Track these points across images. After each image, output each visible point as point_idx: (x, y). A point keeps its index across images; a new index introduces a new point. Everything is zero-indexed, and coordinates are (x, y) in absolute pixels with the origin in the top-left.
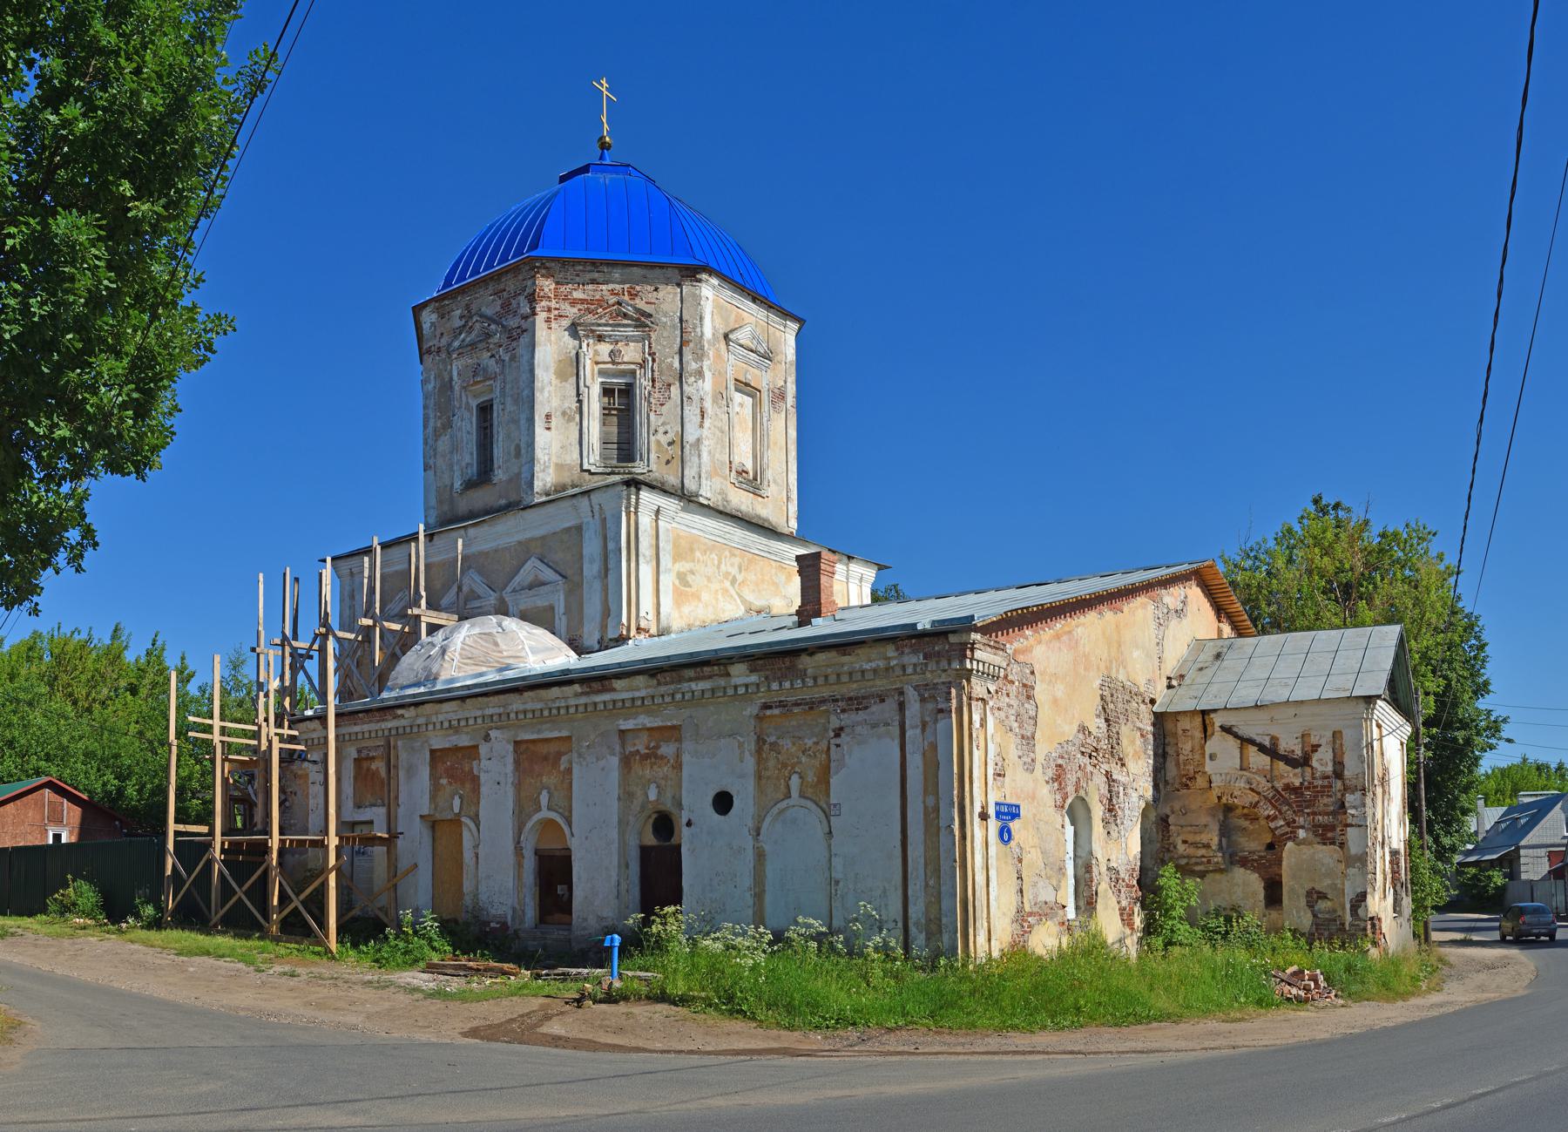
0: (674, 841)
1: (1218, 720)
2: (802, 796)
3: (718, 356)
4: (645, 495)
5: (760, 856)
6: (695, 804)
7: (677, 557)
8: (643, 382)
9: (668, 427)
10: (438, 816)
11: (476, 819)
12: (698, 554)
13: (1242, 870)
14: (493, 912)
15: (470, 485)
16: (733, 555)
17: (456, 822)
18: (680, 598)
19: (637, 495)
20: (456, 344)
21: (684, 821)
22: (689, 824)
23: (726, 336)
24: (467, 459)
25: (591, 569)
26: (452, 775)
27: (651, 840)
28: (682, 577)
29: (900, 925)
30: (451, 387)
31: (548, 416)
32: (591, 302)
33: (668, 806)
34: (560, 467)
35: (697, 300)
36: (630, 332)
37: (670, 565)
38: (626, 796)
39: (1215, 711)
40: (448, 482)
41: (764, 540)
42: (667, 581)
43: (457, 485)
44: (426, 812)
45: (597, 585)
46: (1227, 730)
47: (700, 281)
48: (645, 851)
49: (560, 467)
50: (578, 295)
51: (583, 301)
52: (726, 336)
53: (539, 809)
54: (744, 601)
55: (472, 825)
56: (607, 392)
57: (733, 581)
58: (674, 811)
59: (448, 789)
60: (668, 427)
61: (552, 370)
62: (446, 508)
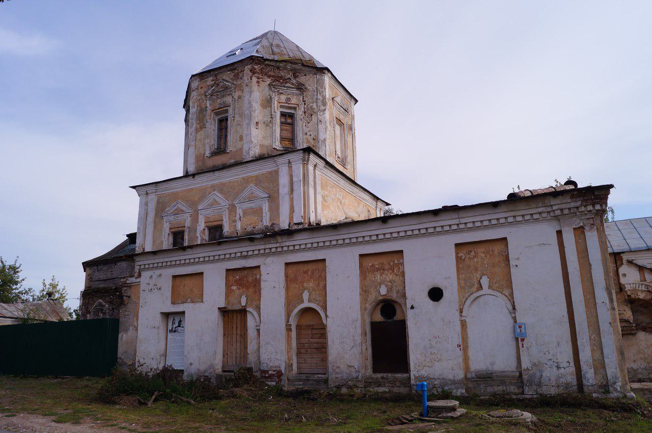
0: (398, 317)
1: (625, 257)
2: (490, 287)
3: (330, 107)
4: (312, 156)
5: (464, 325)
6: (416, 293)
7: (322, 188)
8: (299, 113)
9: (311, 133)
10: (230, 308)
11: (258, 308)
12: (329, 188)
13: (643, 333)
14: (271, 364)
15: (214, 154)
16: (340, 191)
17: (243, 312)
18: (324, 207)
19: (309, 155)
20: (210, 92)
21: (409, 306)
22: (412, 307)
23: (333, 99)
24: (213, 142)
25: (284, 190)
26: (240, 283)
27: (379, 318)
28: (323, 197)
29: (572, 364)
30: (206, 110)
31: (257, 123)
32: (278, 77)
33: (394, 296)
34: (262, 146)
35: (323, 81)
36: (295, 91)
37: (320, 191)
38: (364, 291)
39: (623, 253)
40: (203, 153)
41: (350, 186)
42: (319, 198)
43: (208, 153)
44: (223, 305)
45: (287, 198)
46: (630, 262)
47: (324, 73)
48: (374, 326)
49: (262, 146)
50: (271, 73)
51: (273, 76)
52: (333, 99)
53: (302, 301)
54: (345, 212)
55: (255, 313)
56: (283, 115)
57: (341, 203)
58: (400, 301)
59: (237, 292)
60: (311, 133)
61: (259, 103)
62: (200, 164)
